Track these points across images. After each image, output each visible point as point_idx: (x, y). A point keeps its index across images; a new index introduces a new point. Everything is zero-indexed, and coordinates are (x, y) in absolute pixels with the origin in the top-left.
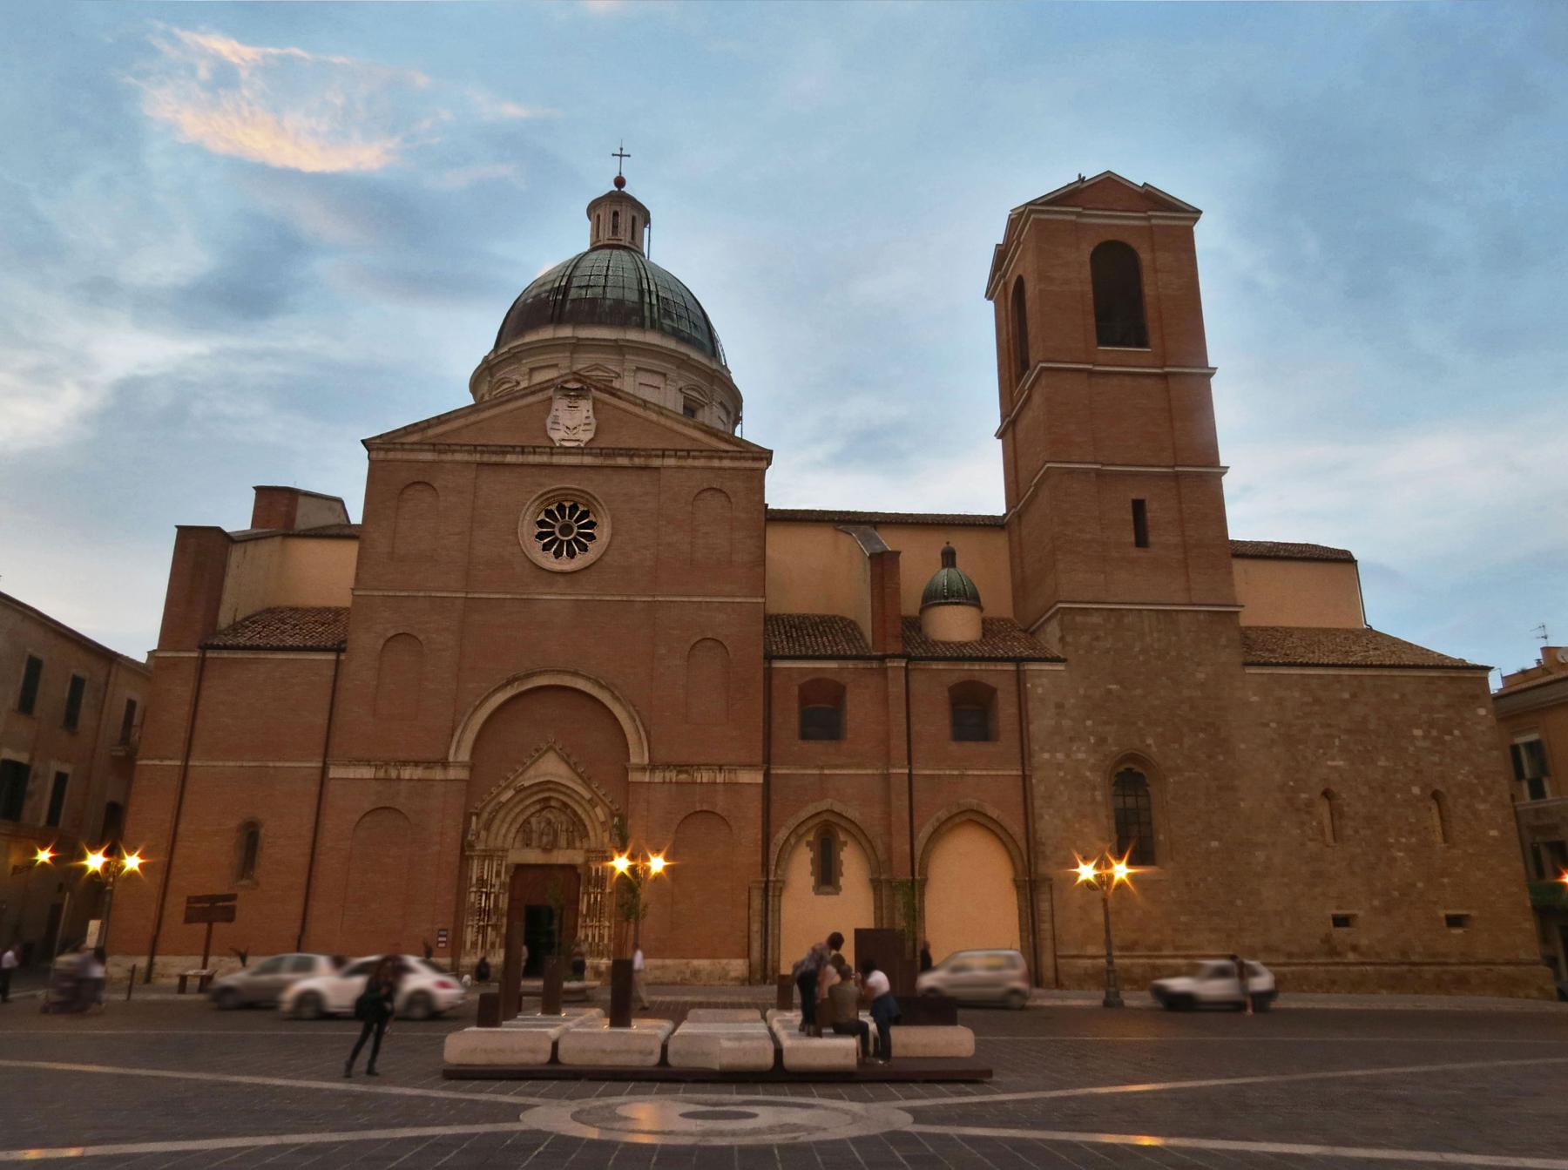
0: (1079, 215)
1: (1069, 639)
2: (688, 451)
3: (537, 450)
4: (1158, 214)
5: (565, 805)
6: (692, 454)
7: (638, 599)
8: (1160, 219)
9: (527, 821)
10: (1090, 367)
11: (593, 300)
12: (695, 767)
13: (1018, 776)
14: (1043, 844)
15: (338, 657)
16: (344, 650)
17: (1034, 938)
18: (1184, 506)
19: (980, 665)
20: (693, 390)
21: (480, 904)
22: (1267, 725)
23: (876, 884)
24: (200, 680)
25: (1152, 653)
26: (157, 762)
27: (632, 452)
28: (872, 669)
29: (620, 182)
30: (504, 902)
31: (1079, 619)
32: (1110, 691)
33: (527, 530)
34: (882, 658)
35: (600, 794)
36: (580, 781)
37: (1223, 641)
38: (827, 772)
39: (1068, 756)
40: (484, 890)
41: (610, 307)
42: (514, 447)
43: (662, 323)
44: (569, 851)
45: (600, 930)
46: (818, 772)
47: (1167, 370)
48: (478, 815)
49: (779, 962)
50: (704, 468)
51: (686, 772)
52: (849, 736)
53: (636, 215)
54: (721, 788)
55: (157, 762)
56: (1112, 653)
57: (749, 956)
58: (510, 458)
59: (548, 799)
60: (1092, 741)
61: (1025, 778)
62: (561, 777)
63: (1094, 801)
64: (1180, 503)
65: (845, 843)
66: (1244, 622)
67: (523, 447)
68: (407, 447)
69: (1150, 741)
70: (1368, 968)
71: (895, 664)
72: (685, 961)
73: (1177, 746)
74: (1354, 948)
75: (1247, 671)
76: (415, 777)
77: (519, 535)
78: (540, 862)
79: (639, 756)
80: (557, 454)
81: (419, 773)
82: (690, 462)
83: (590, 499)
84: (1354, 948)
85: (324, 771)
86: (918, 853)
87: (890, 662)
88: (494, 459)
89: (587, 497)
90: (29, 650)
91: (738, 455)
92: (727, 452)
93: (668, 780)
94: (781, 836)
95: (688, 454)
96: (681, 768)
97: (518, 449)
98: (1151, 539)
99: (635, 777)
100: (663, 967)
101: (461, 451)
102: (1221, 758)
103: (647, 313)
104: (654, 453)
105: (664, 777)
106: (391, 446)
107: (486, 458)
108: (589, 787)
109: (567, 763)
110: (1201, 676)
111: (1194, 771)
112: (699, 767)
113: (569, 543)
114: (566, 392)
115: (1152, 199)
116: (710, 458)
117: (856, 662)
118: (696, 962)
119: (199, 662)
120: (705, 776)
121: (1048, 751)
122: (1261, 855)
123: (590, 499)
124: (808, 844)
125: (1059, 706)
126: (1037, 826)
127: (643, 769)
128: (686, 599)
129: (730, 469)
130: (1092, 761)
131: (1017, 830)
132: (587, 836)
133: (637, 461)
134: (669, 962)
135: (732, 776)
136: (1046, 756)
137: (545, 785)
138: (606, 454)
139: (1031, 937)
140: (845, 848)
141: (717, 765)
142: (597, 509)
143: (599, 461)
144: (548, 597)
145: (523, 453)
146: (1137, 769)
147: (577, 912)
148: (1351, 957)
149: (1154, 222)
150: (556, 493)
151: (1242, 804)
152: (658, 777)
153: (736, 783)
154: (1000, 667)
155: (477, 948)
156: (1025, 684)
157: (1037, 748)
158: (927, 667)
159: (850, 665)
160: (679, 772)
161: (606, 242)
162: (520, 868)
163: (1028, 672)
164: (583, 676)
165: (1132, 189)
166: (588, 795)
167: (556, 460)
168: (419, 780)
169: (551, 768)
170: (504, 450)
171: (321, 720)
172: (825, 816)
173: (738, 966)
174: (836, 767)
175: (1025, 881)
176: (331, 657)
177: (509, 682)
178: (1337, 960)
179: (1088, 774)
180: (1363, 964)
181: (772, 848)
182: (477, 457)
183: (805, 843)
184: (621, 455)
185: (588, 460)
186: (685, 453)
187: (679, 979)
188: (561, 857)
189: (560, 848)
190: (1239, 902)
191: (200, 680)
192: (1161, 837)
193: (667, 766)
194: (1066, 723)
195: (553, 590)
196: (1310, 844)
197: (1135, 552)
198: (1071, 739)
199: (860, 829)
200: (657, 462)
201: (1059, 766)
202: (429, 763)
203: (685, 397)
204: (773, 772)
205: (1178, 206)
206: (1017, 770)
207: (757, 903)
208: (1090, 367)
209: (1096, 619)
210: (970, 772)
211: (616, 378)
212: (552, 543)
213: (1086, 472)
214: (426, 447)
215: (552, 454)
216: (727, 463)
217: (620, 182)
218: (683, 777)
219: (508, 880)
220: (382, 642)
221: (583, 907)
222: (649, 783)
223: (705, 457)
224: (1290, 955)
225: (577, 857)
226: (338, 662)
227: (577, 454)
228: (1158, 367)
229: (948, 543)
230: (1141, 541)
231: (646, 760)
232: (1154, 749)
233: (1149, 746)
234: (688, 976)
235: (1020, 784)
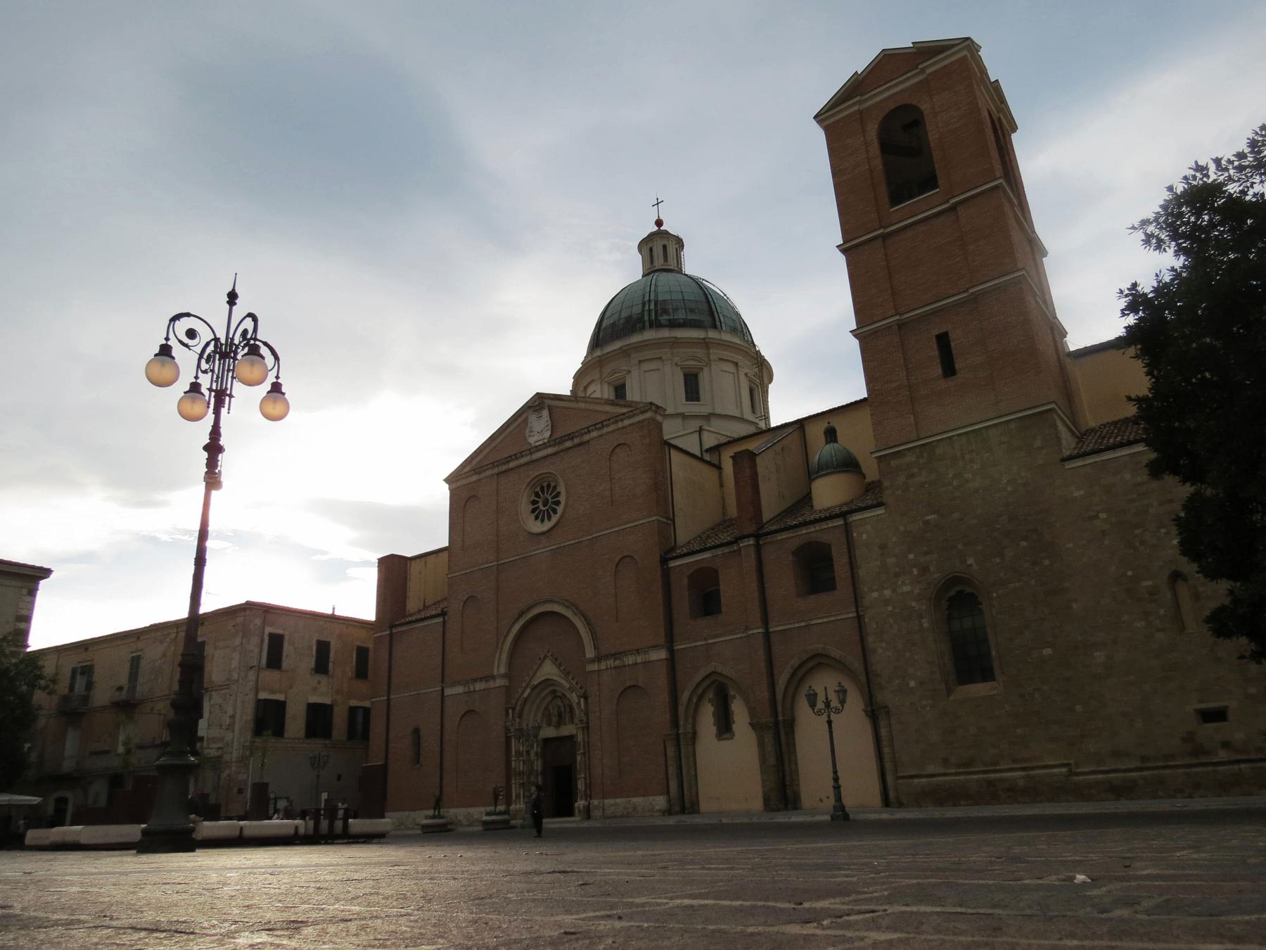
0: (860, 102)
2: (602, 422)
4: (930, 62)
6: (604, 423)
7: (584, 539)
8: (932, 66)
9: (547, 708)
10: (881, 231)
12: (623, 654)
13: (854, 617)
15: (444, 618)
19: (815, 527)
20: (687, 360)
21: (519, 768)
22: (1096, 517)
26: (378, 699)
27: (572, 435)
28: (734, 551)
29: (659, 223)
30: (538, 765)
31: (893, 463)
32: (927, 523)
33: (525, 507)
37: (1038, 443)
38: (710, 641)
39: (894, 591)
40: (521, 758)
42: (511, 456)
43: (660, 320)
46: (704, 643)
48: (514, 709)
49: (697, 796)
50: (613, 431)
53: (666, 242)
55: (378, 699)
57: (668, 793)
58: (512, 465)
60: (915, 573)
61: (859, 618)
65: (734, 697)
67: (515, 455)
69: (970, 561)
70: (1242, 766)
71: (746, 544)
72: (628, 799)
73: (998, 560)
74: (1226, 745)
75: (1067, 467)
79: (590, 653)
80: (534, 452)
82: (605, 430)
84: (1226, 745)
86: (779, 696)
87: (741, 543)
88: (504, 468)
90: (357, 643)
91: (632, 414)
92: (624, 414)
93: (609, 667)
94: (684, 697)
95: (602, 424)
96: (615, 656)
98: (958, 365)
100: (615, 804)
101: (488, 469)
102: (1047, 562)
104: (583, 432)
112: (625, 653)
115: (925, 52)
116: (616, 422)
117: (722, 548)
118: (635, 800)
120: (629, 660)
122: (1099, 656)
124: (710, 700)
125: (883, 547)
127: (592, 661)
128: (610, 531)
129: (630, 425)
130: (917, 591)
131: (858, 666)
133: (577, 441)
134: (618, 801)
135: (647, 656)
136: (875, 595)
140: (734, 700)
141: (635, 650)
144: (538, 552)
145: (517, 459)
148: (1223, 755)
149: (928, 71)
150: (536, 480)
151: (1075, 606)
153: (649, 662)
154: (831, 524)
155: (520, 798)
156: (852, 535)
157: (866, 589)
158: (774, 539)
159: (719, 552)
160: (615, 659)
161: (661, 267)
162: (547, 741)
164: (556, 602)
165: (907, 53)
168: (484, 690)
169: (549, 670)
173: (660, 801)
176: (440, 620)
177: (520, 616)
178: (1204, 760)
179: (914, 604)
180: (1238, 762)
181: (778, 690)
182: (496, 470)
183: (707, 699)
186: (600, 425)
187: (625, 813)
189: (565, 724)
190: (1079, 708)
193: (607, 657)
195: (541, 546)
196: (1159, 635)
198: (897, 575)
200: (586, 438)
203: (681, 368)
204: (676, 648)
205: (946, 45)
206: (852, 612)
207: (671, 751)
208: (881, 231)
209: (910, 458)
211: (628, 374)
212: (539, 513)
213: (889, 327)
215: (531, 454)
216: (627, 422)
217: (659, 223)
218: (617, 663)
219: (539, 750)
222: (598, 670)
223: (613, 423)
224: (1144, 759)
226: (444, 622)
227: (544, 448)
228: (945, 203)
229: (829, 423)
230: (949, 369)
232: (975, 567)
233: (970, 565)
234: (630, 810)
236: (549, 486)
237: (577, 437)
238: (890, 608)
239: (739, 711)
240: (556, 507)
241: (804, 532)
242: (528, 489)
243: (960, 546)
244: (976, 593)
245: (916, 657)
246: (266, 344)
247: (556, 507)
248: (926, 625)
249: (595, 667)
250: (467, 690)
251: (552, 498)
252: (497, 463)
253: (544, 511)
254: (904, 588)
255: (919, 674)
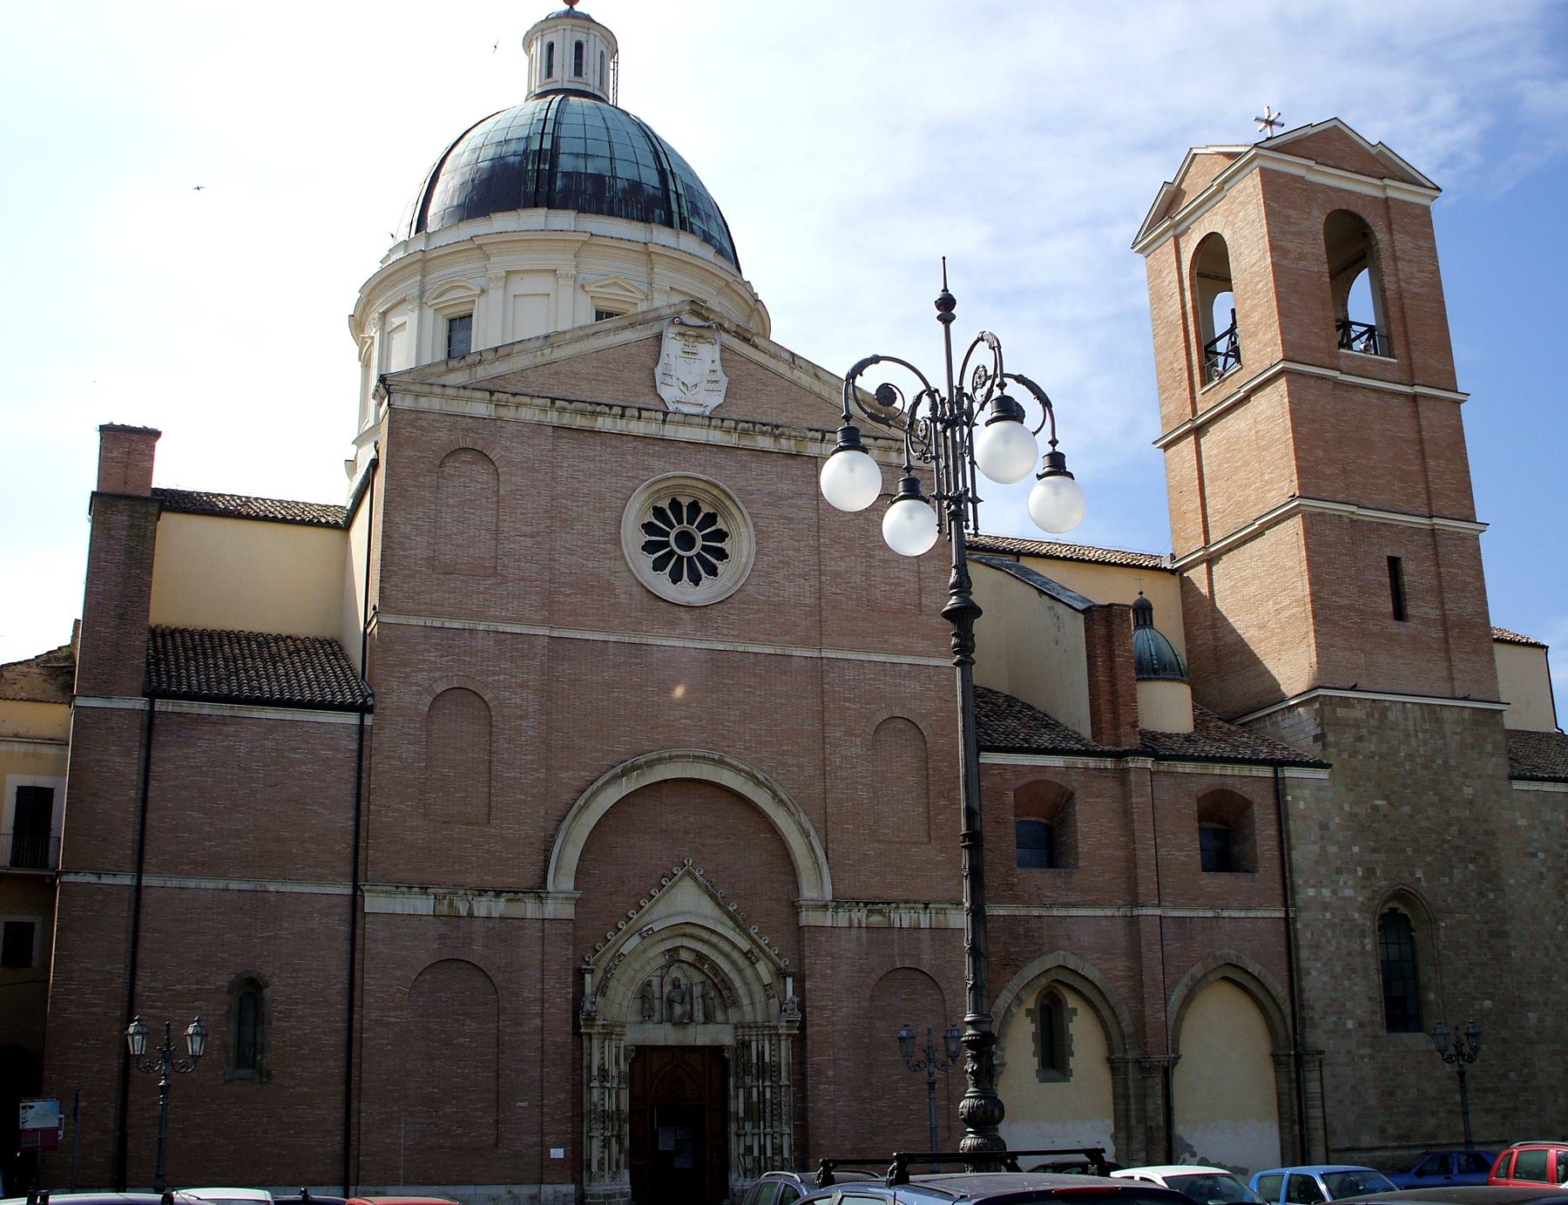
1: (1331, 738)
3: (644, 414)
5: (701, 957)
11: (598, 179)
14: (1312, 1008)
16: (370, 710)
17: (1301, 1130)
18: (1442, 570)
22: (1534, 855)
23: (1115, 1065)
24: (148, 747)
25: (1418, 760)
31: (1340, 712)
32: (1375, 808)
34: (1120, 756)
35: (762, 943)
36: (731, 924)
39: (1334, 892)
41: (624, 190)
42: (611, 407)
44: (710, 1027)
45: (773, 1138)
47: (1418, 389)
51: (880, 912)
52: (1081, 863)
54: (925, 936)
56: (1377, 758)
59: (676, 949)
60: (1360, 874)
61: (1287, 921)
62: (705, 917)
63: (1363, 952)
64: (1438, 565)
65: (1074, 1011)
66: (1511, 722)
68: (449, 391)
73: (1446, 880)
76: (495, 914)
77: (623, 544)
78: (671, 1043)
81: (499, 907)
83: (722, 498)
85: (355, 901)
88: (580, 422)
89: (716, 492)
96: (871, 905)
97: (617, 410)
98: (1410, 610)
99: (809, 918)
102: (1491, 896)
103: (674, 207)
105: (850, 919)
106: (427, 389)
107: (566, 420)
108: (745, 932)
109: (713, 897)
110: (1468, 791)
111: (1465, 913)
113: (672, 553)
114: (682, 329)
119: (145, 718)
121: (1313, 887)
123: (722, 498)
125: (1324, 826)
126: (1303, 984)
130: (1360, 899)
132: (735, 1002)
133: (785, 445)
135: (941, 917)
136: (1311, 892)
137: (686, 929)
138: (743, 429)
139: (1297, 1128)
140: (1074, 1018)
142: (731, 514)
143: (733, 440)
146: (1403, 910)
147: (725, 1117)
151: (1513, 954)
152: (842, 919)
157: (1301, 882)
159: (1080, 762)
160: (871, 912)
162: (642, 1053)
163: (1287, 781)
166: (745, 945)
167: (670, 432)
170: (596, 408)
171: (345, 820)
172: (1054, 975)
174: (1067, 905)
175: (1289, 1055)
176: (352, 719)
179: (1356, 915)
182: (552, 417)
184: (763, 433)
185: (716, 437)
188: (701, 1035)
191: (148, 747)
192: (1432, 996)
194: (1332, 849)
197: (1393, 626)
198: (1339, 871)
199: (1102, 993)
201: (1326, 907)
202: (516, 893)
210: (1225, 914)
214: (479, 394)
220: (429, 700)
221: (738, 1105)
225: (723, 1035)
230: (1399, 614)
231: (829, 896)
235: (1283, 929)
236: (676, 505)
237: (789, 438)
238: (1328, 916)
239: (1083, 1033)
240: (649, 538)
241: (1217, 771)
242: (646, 494)
243: (1409, 851)
244: (1409, 916)
245: (1355, 988)
246: (1020, 379)
247: (649, 538)
248: (1369, 947)
249: (826, 919)
250: (444, 908)
251: (672, 527)
252: (565, 404)
253: (667, 544)
254: (1346, 891)
255: (1358, 1012)
